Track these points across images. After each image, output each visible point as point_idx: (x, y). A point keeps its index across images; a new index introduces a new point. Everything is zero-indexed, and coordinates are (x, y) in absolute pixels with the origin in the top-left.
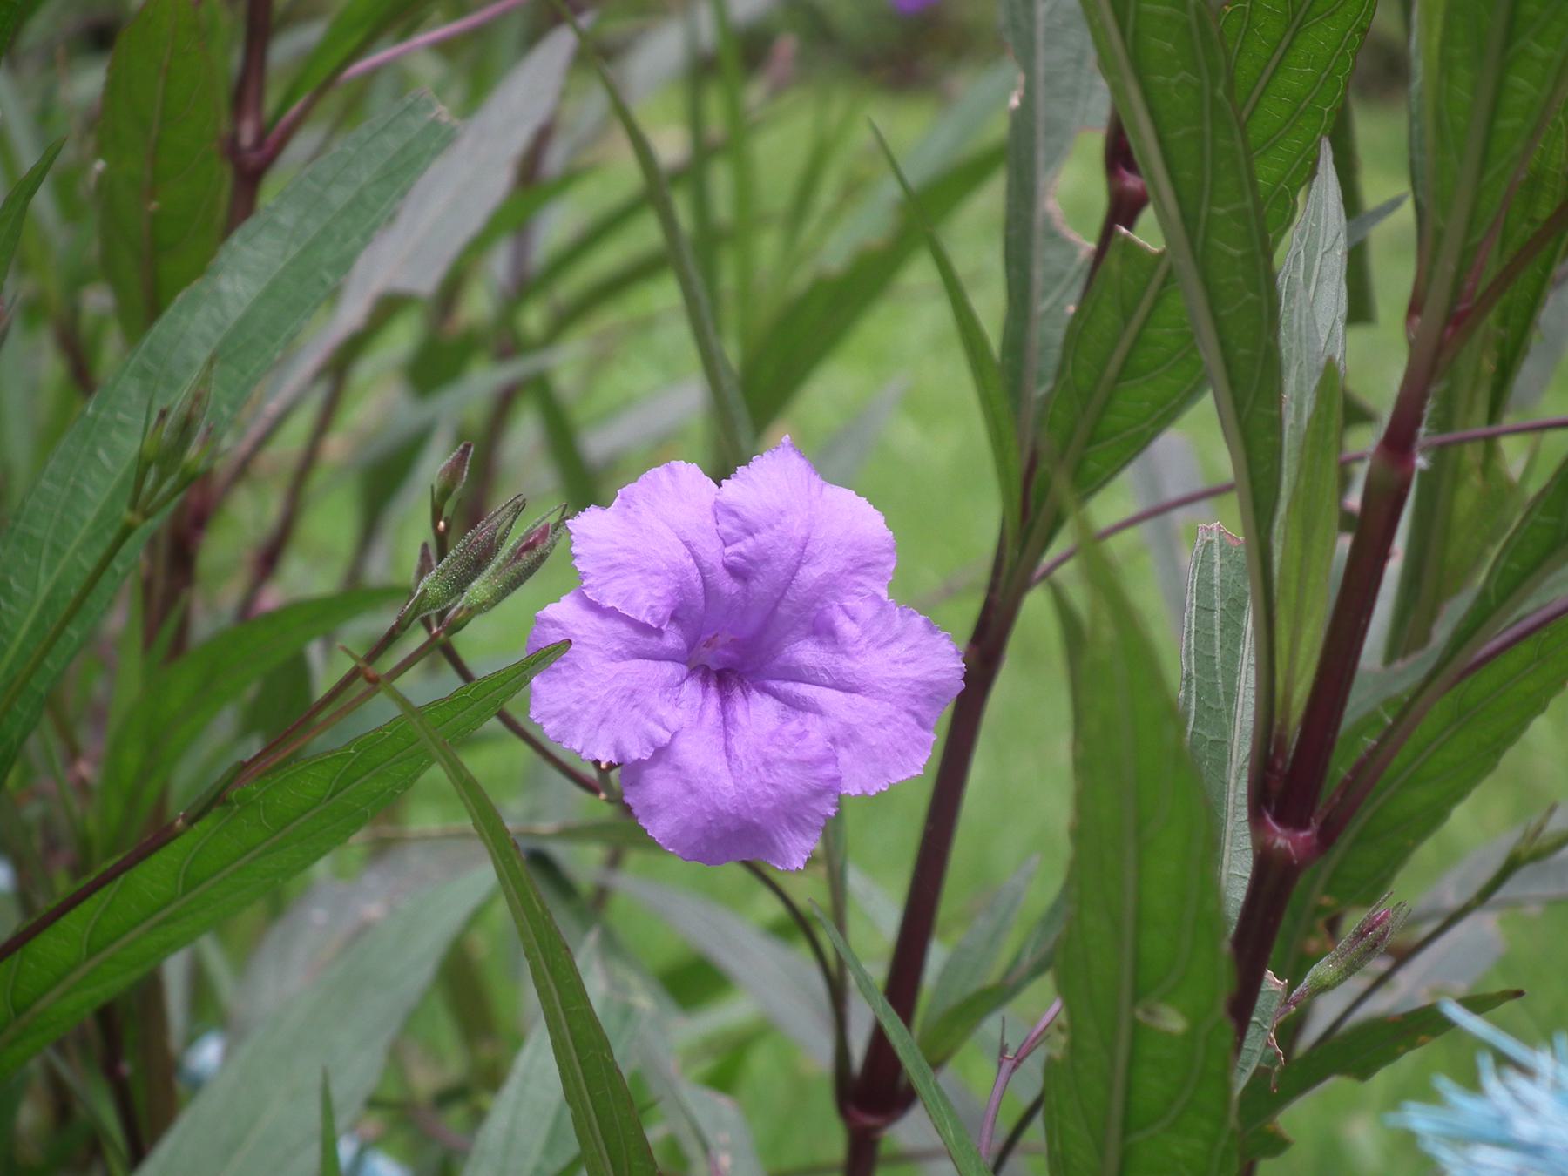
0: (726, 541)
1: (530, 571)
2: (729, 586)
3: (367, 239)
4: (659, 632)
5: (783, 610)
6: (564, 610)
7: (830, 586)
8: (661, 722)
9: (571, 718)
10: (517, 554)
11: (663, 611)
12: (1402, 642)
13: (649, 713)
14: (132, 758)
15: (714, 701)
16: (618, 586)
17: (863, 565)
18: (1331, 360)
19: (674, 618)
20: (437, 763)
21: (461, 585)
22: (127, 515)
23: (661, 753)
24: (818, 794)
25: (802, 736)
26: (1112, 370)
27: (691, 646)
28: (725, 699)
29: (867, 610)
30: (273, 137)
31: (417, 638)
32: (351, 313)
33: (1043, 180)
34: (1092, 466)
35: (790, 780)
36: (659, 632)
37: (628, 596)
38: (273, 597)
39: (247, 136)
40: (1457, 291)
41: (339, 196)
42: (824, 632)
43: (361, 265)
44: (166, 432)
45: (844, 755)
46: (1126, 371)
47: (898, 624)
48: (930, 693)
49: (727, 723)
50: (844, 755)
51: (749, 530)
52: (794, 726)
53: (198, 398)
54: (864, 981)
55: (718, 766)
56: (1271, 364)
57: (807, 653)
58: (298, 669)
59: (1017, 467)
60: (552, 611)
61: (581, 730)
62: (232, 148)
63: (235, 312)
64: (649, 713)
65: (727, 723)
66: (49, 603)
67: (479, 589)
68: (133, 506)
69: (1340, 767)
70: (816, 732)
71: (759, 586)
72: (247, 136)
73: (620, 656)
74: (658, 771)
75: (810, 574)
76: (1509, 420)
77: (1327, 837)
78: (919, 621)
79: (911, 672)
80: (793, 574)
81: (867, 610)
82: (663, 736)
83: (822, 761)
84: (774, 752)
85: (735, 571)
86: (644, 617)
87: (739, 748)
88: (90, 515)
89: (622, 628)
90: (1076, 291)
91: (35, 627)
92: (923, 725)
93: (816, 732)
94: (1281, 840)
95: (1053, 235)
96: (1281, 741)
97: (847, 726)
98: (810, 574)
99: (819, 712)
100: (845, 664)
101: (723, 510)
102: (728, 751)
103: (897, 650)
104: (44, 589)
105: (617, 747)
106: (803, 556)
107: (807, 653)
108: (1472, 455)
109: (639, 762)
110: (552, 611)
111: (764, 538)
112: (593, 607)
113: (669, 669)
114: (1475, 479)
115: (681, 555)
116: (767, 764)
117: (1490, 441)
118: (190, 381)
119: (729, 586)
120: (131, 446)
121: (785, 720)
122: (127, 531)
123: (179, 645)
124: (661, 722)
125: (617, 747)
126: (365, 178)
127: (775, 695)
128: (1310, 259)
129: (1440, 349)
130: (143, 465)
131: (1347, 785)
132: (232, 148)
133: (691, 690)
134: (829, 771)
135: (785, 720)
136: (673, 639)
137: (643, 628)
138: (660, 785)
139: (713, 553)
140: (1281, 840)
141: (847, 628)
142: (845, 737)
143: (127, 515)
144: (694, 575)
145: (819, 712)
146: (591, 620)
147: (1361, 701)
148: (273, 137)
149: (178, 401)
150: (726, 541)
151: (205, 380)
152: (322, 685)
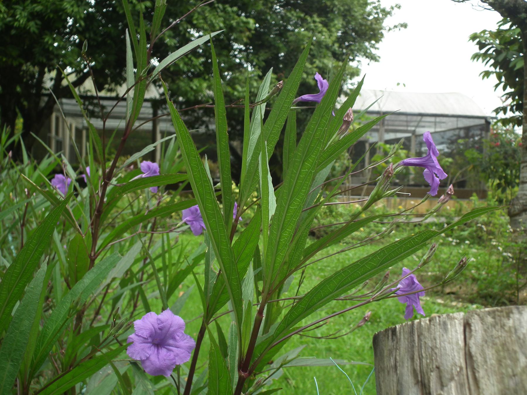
0: (159, 324)
1: (129, 328)
2: (159, 331)
3: (107, 274)
4: (147, 339)
5: (167, 335)
6: (132, 336)
7: (175, 331)
8: (148, 353)
9: (133, 353)
10: (127, 326)
11: (148, 336)
12: (266, 331)
13: (146, 352)
14: (70, 351)
15: (156, 350)
16: (141, 332)
17: (180, 328)
18: (250, 301)
19: (150, 336)
20: (109, 364)
21: (117, 331)
22: (67, 317)
23: (148, 358)
24: (172, 365)
25: (170, 355)
26: (220, 293)
27: (153, 341)
28: (158, 349)
29: (180, 335)
30: (97, 254)
31: (111, 338)
32: (108, 280)
33: (211, 263)
34: (217, 307)
35: (168, 362)
36: (147, 339)
37: (143, 334)
38: (95, 325)
39: (92, 255)
40: (269, 290)
41: (103, 267)
42: (174, 339)
43: (110, 273)
44: (74, 304)
45: (177, 358)
46: (222, 293)
47: (185, 337)
48: (190, 348)
49: (158, 353)
50: (177, 358)
51: (162, 323)
52: (169, 354)
53: (79, 299)
54: (182, 386)
55: (157, 360)
56: (241, 300)
57: (171, 342)
58: (98, 336)
59: (206, 308)
60: (131, 336)
61: (135, 355)
62: (90, 256)
63: (86, 285)
64: (146, 352)
65: (158, 353)
66: (55, 330)
67: (120, 331)
68: (68, 315)
69: (251, 363)
70: (172, 355)
71: (164, 331)
72: (92, 255)
73: (142, 343)
74: (147, 361)
75: (172, 329)
76: (280, 299)
77: (250, 374)
78: (189, 336)
79: (187, 345)
80: (169, 329)
81: (180, 335)
82: (148, 356)
83: (173, 359)
84: (166, 358)
85: (160, 329)
86: (145, 337)
87: (160, 357)
88: (62, 316)
89: (142, 338)
90: (215, 280)
91: (52, 334)
92: (189, 353)
93: (172, 355)
94: (243, 374)
95: (212, 271)
96: (243, 359)
97: (177, 354)
98: (172, 329)
99: (173, 351)
100: (177, 344)
101: (158, 319)
102: (158, 358)
103: (185, 341)
104: (54, 328)
105: (141, 358)
106: (171, 327)
107: (171, 342)
108: (275, 303)
109: (144, 360)
110: (131, 336)
111: (164, 324)
112: (137, 335)
113: (149, 345)
114: (275, 307)
115: (151, 327)
116: (164, 360)
117: (278, 301)
118: (79, 295)
119: (159, 331)
120: (69, 305)
121: (167, 353)
122: (67, 319)
123: (79, 332)
124: (148, 353)
125: (141, 358)
126: (107, 265)
127: (166, 348)
128: (248, 280)
129: (267, 298)
130: (70, 309)
131: (253, 366)
132: (90, 256)
133: (153, 348)
134: (174, 361)
135: (167, 353)
136: (150, 340)
137: (145, 338)
138: (148, 363)
139: (156, 326)
140: (243, 374)
141: (177, 338)
142: (177, 355)
143: (67, 317)
144: (153, 330)
145: (173, 351)
146: (137, 337)
147: (258, 341)
148: (97, 254)
149: (76, 299)
150: (159, 324)
151: (80, 296)
152: (102, 340)
